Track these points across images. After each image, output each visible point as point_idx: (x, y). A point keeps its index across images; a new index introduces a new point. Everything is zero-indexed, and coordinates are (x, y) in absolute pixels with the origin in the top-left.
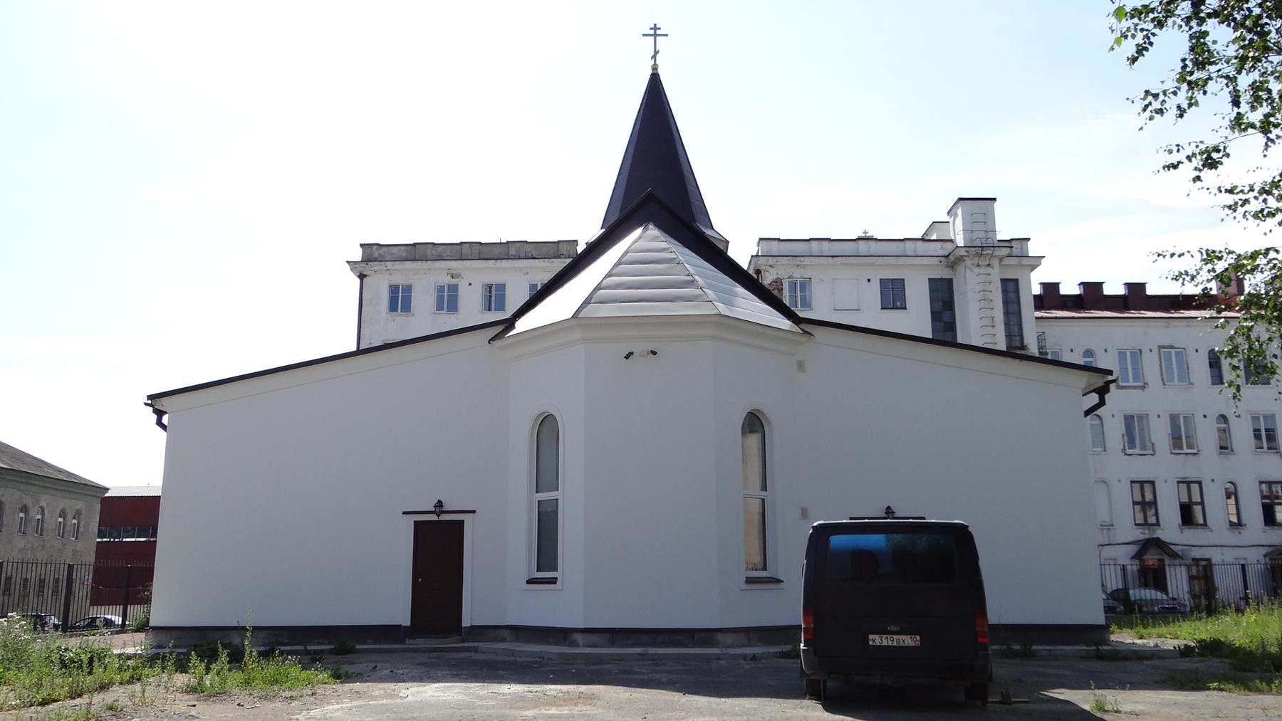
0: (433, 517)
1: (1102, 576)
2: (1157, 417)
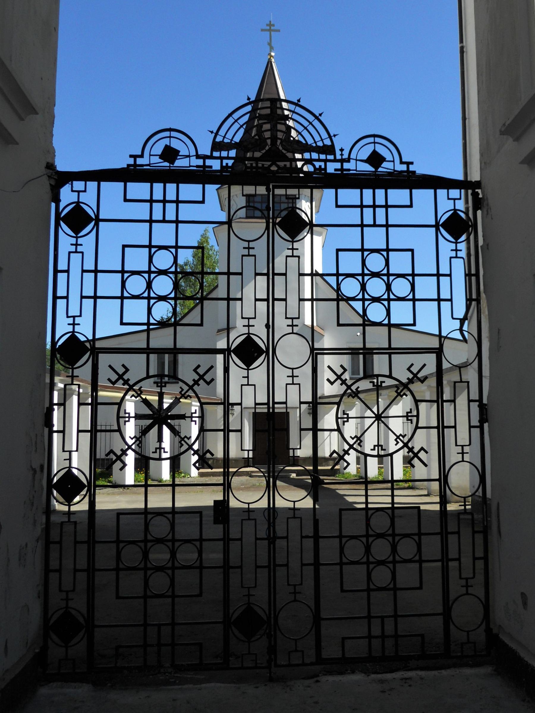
0: (169, 168)
1: (462, 51)
2: (43, 79)
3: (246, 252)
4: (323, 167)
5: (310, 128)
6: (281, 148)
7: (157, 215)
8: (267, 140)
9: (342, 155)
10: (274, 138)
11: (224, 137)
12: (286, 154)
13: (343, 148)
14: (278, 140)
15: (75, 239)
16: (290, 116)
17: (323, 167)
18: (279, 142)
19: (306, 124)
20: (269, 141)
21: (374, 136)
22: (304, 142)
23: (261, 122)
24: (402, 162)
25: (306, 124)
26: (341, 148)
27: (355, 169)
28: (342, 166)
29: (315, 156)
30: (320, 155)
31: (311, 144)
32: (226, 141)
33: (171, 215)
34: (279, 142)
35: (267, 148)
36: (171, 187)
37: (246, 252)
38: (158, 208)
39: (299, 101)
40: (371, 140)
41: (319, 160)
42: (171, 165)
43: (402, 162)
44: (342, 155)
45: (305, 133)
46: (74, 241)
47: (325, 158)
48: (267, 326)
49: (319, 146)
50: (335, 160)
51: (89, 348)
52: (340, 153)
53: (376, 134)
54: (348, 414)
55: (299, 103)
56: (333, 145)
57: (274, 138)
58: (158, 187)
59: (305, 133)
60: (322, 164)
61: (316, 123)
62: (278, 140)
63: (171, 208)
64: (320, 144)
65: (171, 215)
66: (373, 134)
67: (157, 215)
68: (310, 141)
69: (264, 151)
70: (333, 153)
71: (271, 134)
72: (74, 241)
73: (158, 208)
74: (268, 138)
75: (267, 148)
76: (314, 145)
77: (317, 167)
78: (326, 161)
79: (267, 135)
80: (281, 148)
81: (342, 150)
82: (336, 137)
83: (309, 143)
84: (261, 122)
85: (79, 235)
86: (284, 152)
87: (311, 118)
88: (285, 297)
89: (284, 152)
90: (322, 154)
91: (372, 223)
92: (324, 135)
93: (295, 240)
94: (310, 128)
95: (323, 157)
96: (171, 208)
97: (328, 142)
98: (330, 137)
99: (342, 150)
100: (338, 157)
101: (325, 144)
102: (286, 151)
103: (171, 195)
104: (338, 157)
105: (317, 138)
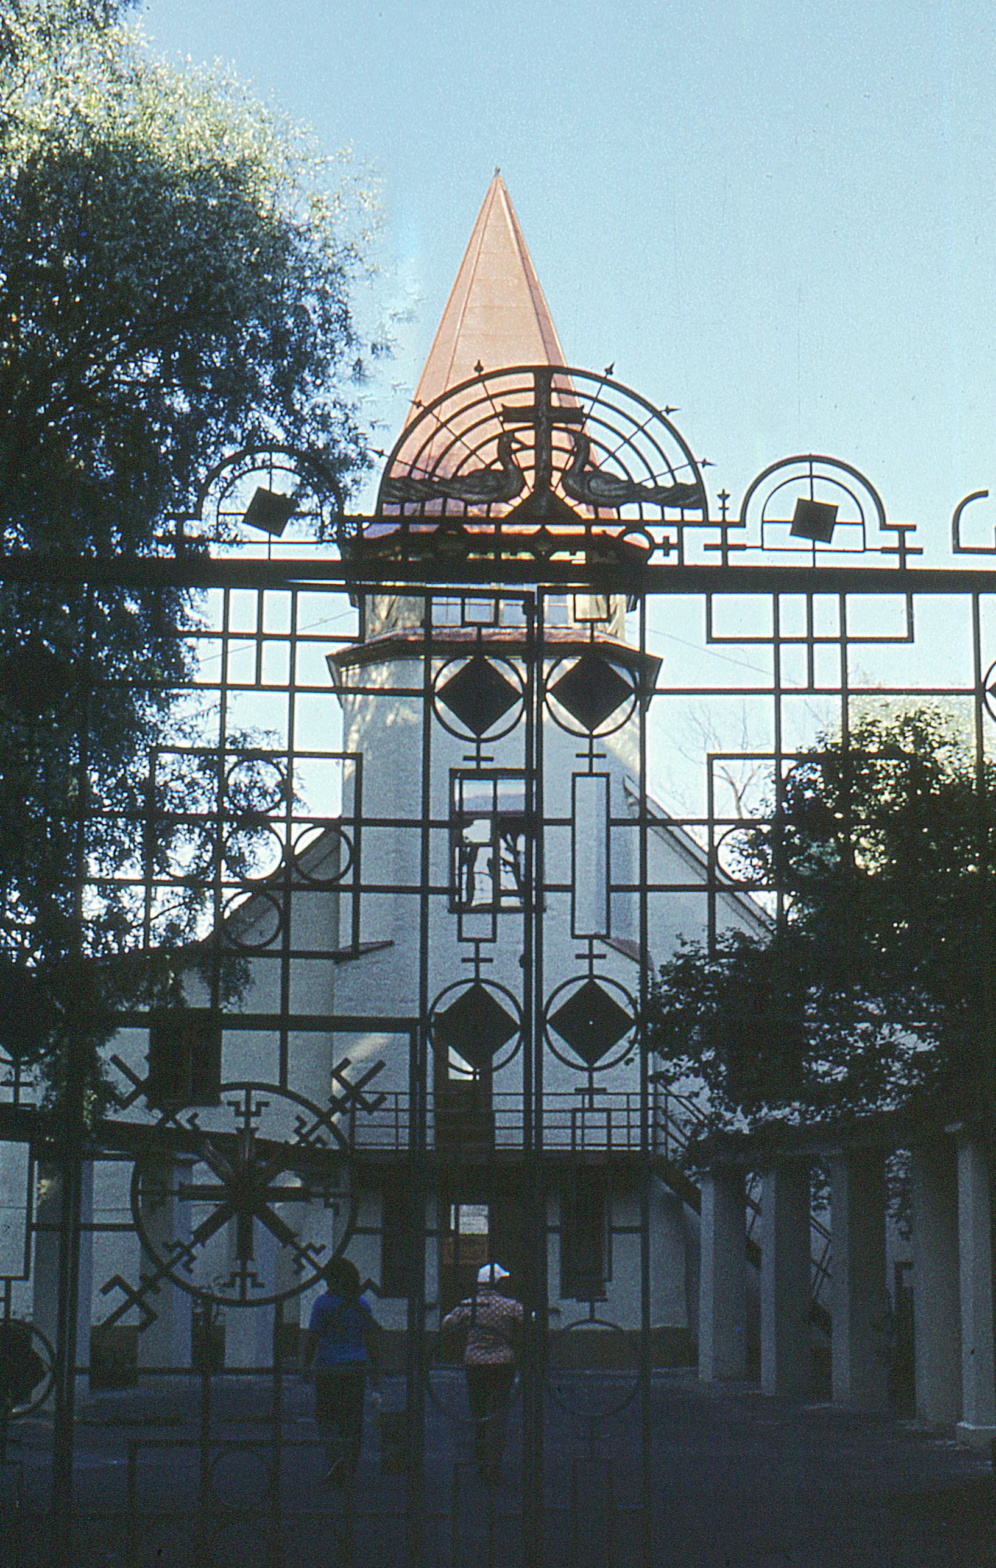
3: (583, 765)
4: (674, 540)
5: (639, 440)
6: (561, 493)
7: (794, 675)
8: (526, 473)
9: (724, 509)
10: (544, 468)
11: (413, 467)
12: (575, 509)
13: (727, 492)
14: (554, 473)
15: (474, 745)
16: (586, 411)
17: (674, 540)
18: (556, 476)
19: (628, 429)
20: (530, 477)
21: (811, 459)
22: (623, 477)
23: (508, 426)
24: (884, 527)
25: (628, 429)
26: (720, 492)
27: (759, 544)
28: (724, 536)
29: (652, 511)
30: (666, 509)
31: (640, 484)
32: (417, 475)
33: (828, 676)
34: (556, 476)
35: (525, 493)
36: (277, 600)
37: (583, 765)
38: (794, 656)
39: (609, 371)
40: (804, 468)
41: (663, 523)
42: (274, 538)
43: (884, 527)
44: (724, 509)
45: (626, 454)
46: (583, 746)
47: (679, 518)
48: (525, 961)
49: (665, 489)
50: (706, 523)
51: (632, 1017)
52: (720, 503)
53: (814, 453)
54: (179, 1244)
55: (483, 373)
56: (699, 485)
57: (544, 468)
58: (793, 603)
59: (626, 454)
60: (672, 533)
61: (655, 427)
62: (554, 473)
63: (827, 656)
64: (666, 482)
65: (828, 676)
66: (807, 453)
67: (794, 675)
68: (640, 475)
69: (516, 502)
70: (701, 503)
71: (538, 457)
72: (583, 746)
73: (794, 656)
74: (528, 468)
75: (525, 493)
76: (650, 484)
77: (659, 540)
78: (681, 525)
79: (526, 459)
80: (561, 493)
81: (724, 497)
82: (380, 450)
83: (636, 480)
84: (508, 426)
85: (484, 736)
86: (570, 502)
87: (641, 415)
88: (569, 882)
89: (570, 502)
90: (673, 505)
91: (253, 682)
92: (677, 458)
93: (484, 736)
94: (639, 440)
95: (673, 514)
96: (827, 656)
97: (687, 477)
98: (692, 463)
99: (724, 497)
100: (715, 515)
101: (679, 480)
102: (575, 499)
103: (827, 625)
104: (715, 515)
105: (659, 467)
